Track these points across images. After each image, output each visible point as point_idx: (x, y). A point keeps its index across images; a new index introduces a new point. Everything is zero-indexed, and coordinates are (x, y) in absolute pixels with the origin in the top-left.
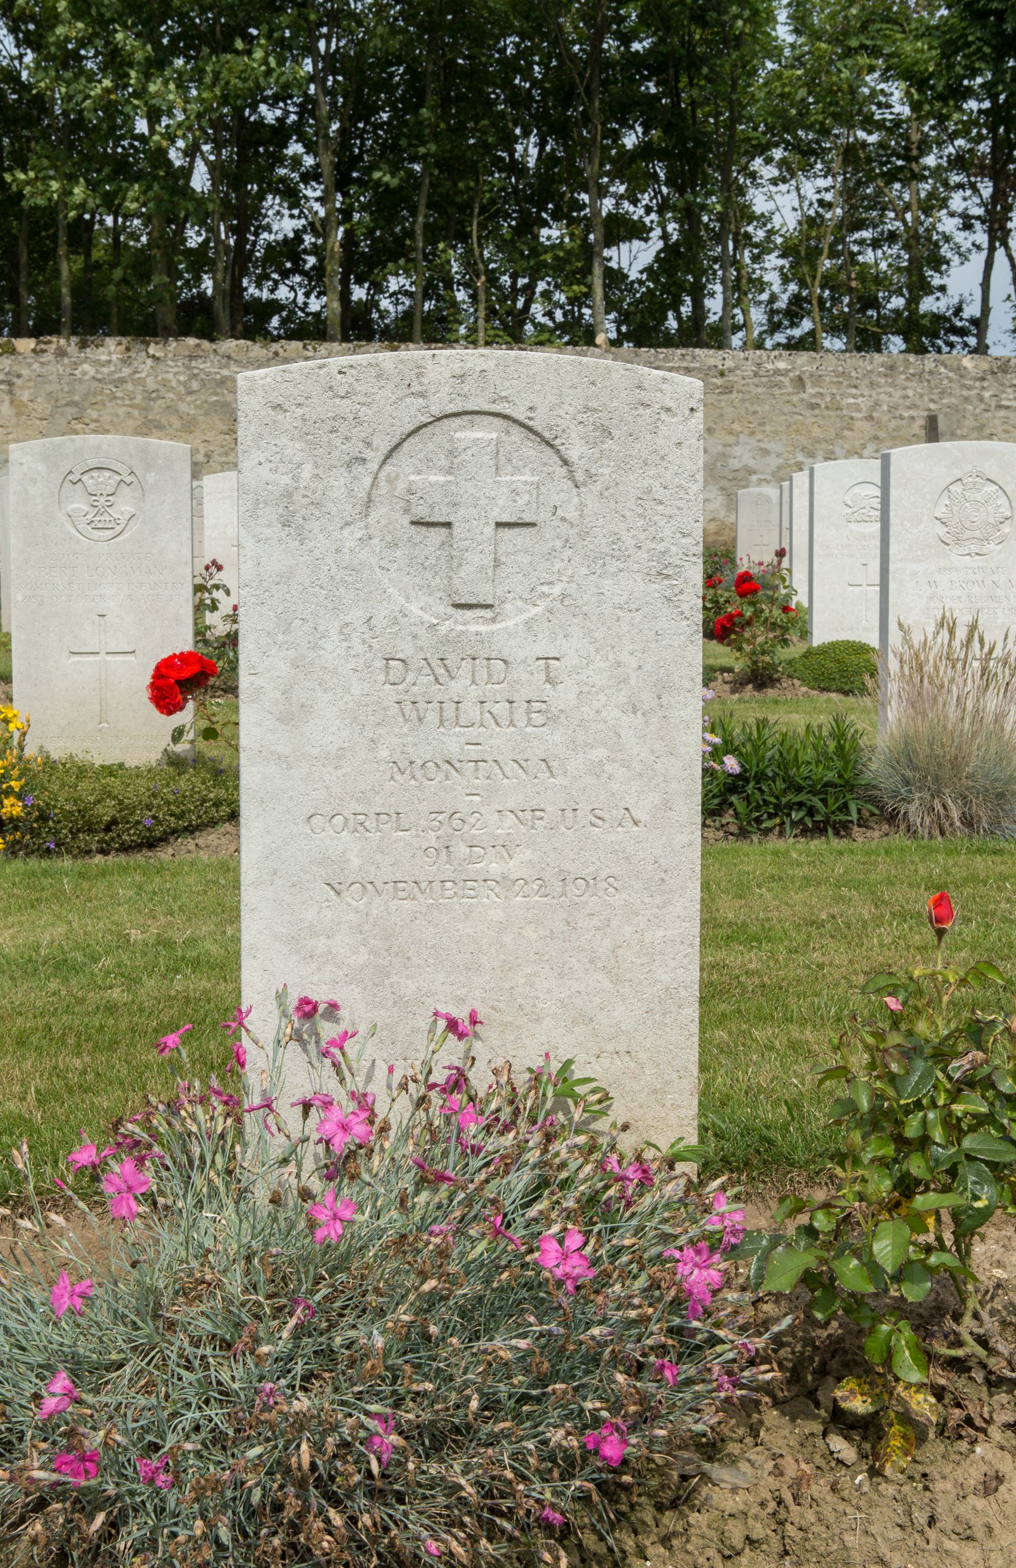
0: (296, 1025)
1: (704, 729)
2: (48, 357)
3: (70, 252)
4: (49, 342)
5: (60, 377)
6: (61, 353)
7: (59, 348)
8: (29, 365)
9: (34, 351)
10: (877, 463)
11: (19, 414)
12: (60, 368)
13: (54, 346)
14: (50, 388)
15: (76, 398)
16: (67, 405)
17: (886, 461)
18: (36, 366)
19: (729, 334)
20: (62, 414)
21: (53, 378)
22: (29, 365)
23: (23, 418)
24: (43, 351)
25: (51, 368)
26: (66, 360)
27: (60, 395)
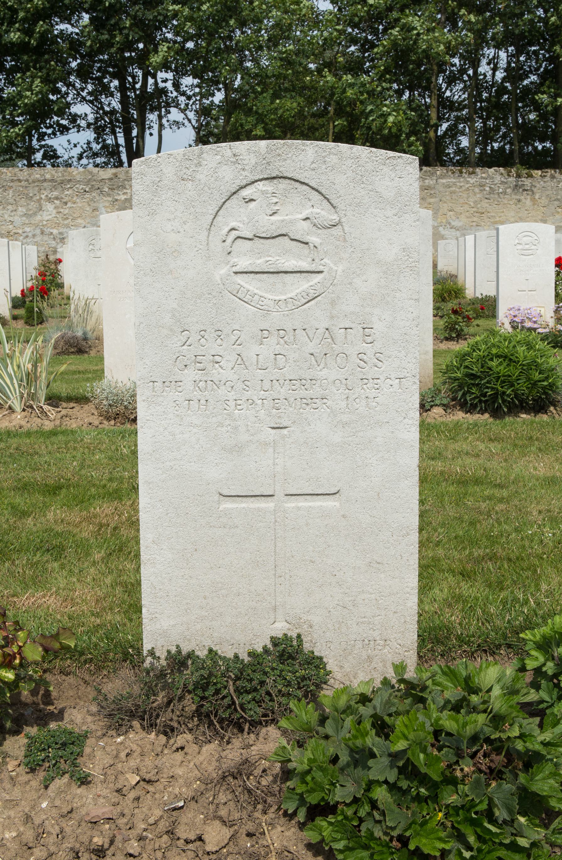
0: (540, 330)
1: (436, 338)
2: (547, 179)
3: (387, 70)
4: (547, 172)
5: (552, 188)
6: (553, 177)
7: (551, 175)
8: (539, 182)
9: (541, 176)
10: (495, 232)
11: (534, 204)
12: (553, 184)
13: (549, 174)
14: (548, 193)
15: (559, 197)
16: (555, 200)
17: (497, 229)
18: (542, 183)
19: (148, 112)
20: (553, 204)
21: (549, 188)
22: (539, 182)
23: (536, 206)
24: (545, 176)
25: (548, 184)
26: (555, 180)
27: (552, 196)
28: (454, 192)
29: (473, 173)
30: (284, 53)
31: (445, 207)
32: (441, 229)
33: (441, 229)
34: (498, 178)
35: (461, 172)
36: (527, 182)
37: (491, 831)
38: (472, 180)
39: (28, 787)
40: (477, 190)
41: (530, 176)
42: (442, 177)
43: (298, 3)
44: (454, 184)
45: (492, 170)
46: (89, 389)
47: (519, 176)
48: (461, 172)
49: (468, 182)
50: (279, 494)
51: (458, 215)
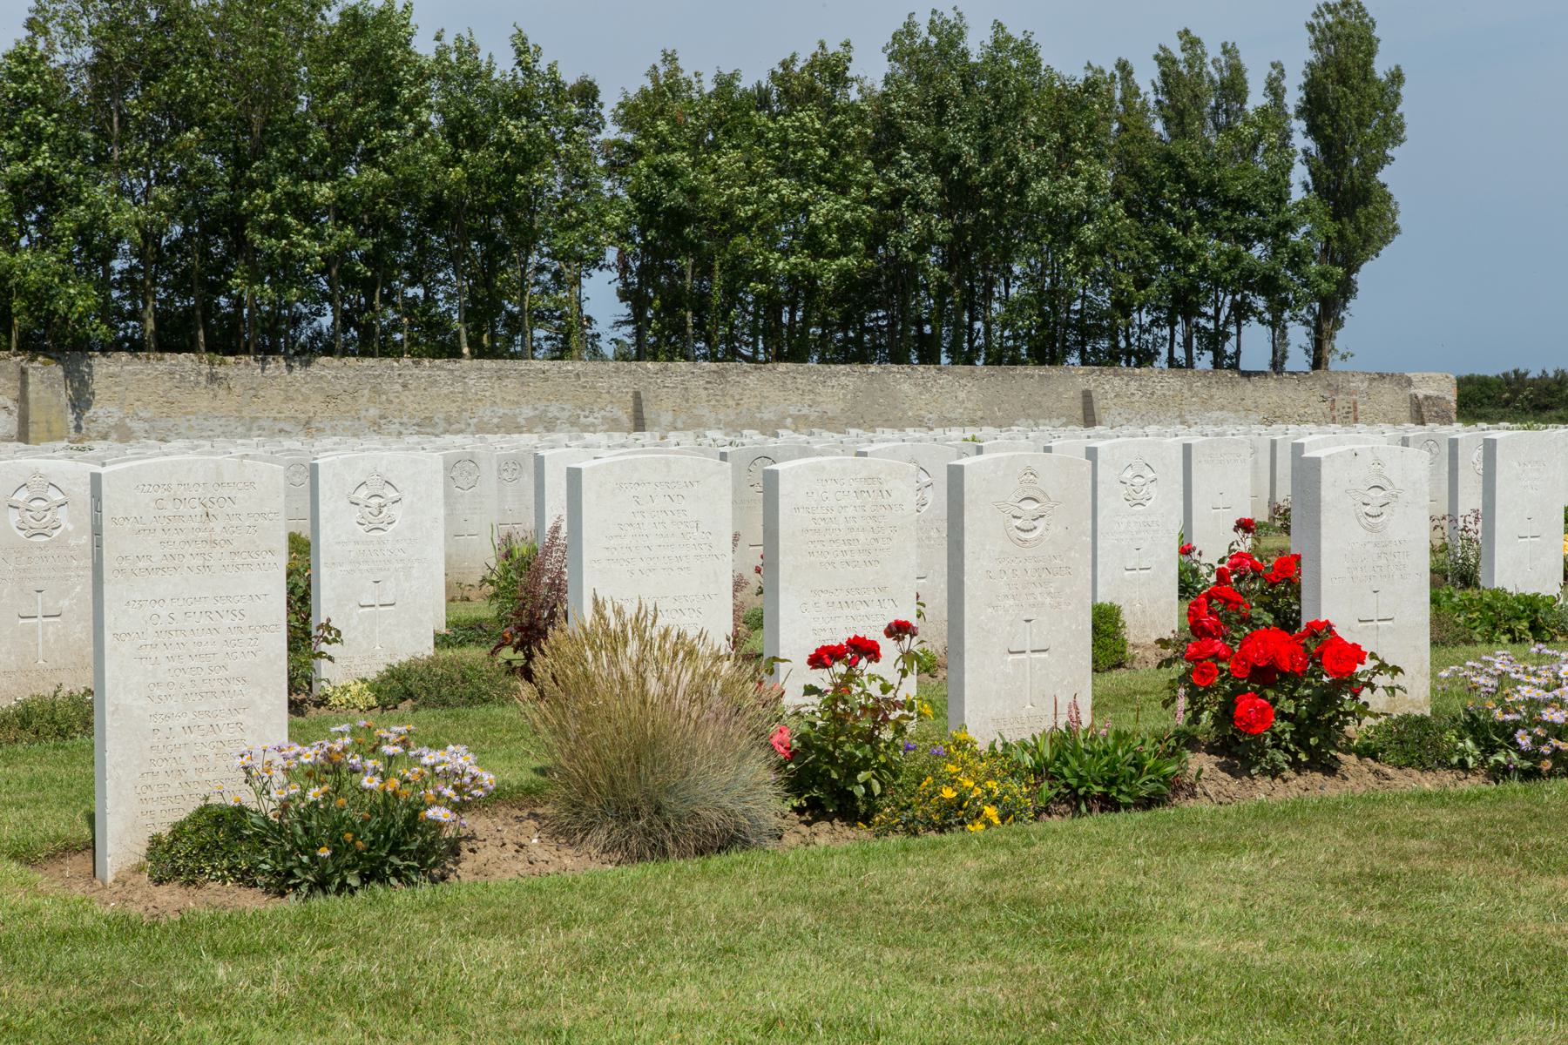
2: (241, 366)
6: (247, 364)
28: (141, 380)
29: (162, 359)
30: (124, 164)
31: (131, 396)
32: (128, 420)
33: (128, 420)
34: (189, 365)
35: (148, 358)
36: (221, 371)
37: (374, 299)
38: (161, 367)
39: (418, 144)
40: (166, 378)
41: (222, 363)
42: (127, 363)
43: (4, 110)
44: (142, 371)
45: (181, 356)
46: (418, 144)
47: (211, 363)
48: (148, 358)
49: (156, 369)
50: (40, 616)
51: (146, 405)
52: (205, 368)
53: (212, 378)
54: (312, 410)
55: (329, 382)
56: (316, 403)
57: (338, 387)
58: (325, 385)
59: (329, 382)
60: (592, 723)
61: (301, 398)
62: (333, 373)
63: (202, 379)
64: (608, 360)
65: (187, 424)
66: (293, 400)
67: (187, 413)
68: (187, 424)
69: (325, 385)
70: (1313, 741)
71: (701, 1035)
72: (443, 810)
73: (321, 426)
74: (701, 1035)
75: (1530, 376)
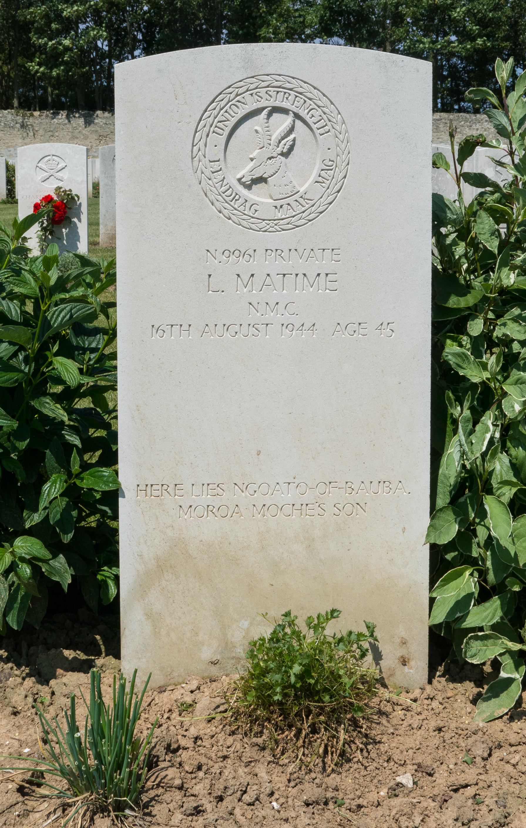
2: (43, 117)
34: (10, 117)
47: (24, 116)
52: (20, 119)
53: (23, 126)
54: (90, 145)
55: (101, 127)
56: (92, 140)
57: (107, 130)
58: (98, 129)
59: (101, 127)
60: (420, 705)
61: (82, 137)
62: (104, 121)
63: (18, 126)
64: (461, 161)
65: (8, 153)
66: (77, 138)
67: (9, 147)
68: (8, 153)
69: (98, 129)
70: (98, 61)
71: (519, 71)
72: (475, 380)
73: (96, 154)
74: (519, 71)
75: (78, 243)
